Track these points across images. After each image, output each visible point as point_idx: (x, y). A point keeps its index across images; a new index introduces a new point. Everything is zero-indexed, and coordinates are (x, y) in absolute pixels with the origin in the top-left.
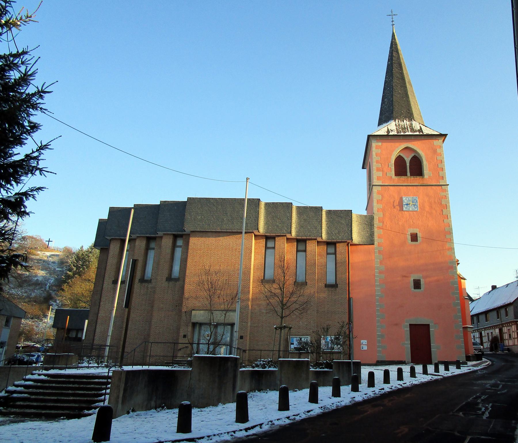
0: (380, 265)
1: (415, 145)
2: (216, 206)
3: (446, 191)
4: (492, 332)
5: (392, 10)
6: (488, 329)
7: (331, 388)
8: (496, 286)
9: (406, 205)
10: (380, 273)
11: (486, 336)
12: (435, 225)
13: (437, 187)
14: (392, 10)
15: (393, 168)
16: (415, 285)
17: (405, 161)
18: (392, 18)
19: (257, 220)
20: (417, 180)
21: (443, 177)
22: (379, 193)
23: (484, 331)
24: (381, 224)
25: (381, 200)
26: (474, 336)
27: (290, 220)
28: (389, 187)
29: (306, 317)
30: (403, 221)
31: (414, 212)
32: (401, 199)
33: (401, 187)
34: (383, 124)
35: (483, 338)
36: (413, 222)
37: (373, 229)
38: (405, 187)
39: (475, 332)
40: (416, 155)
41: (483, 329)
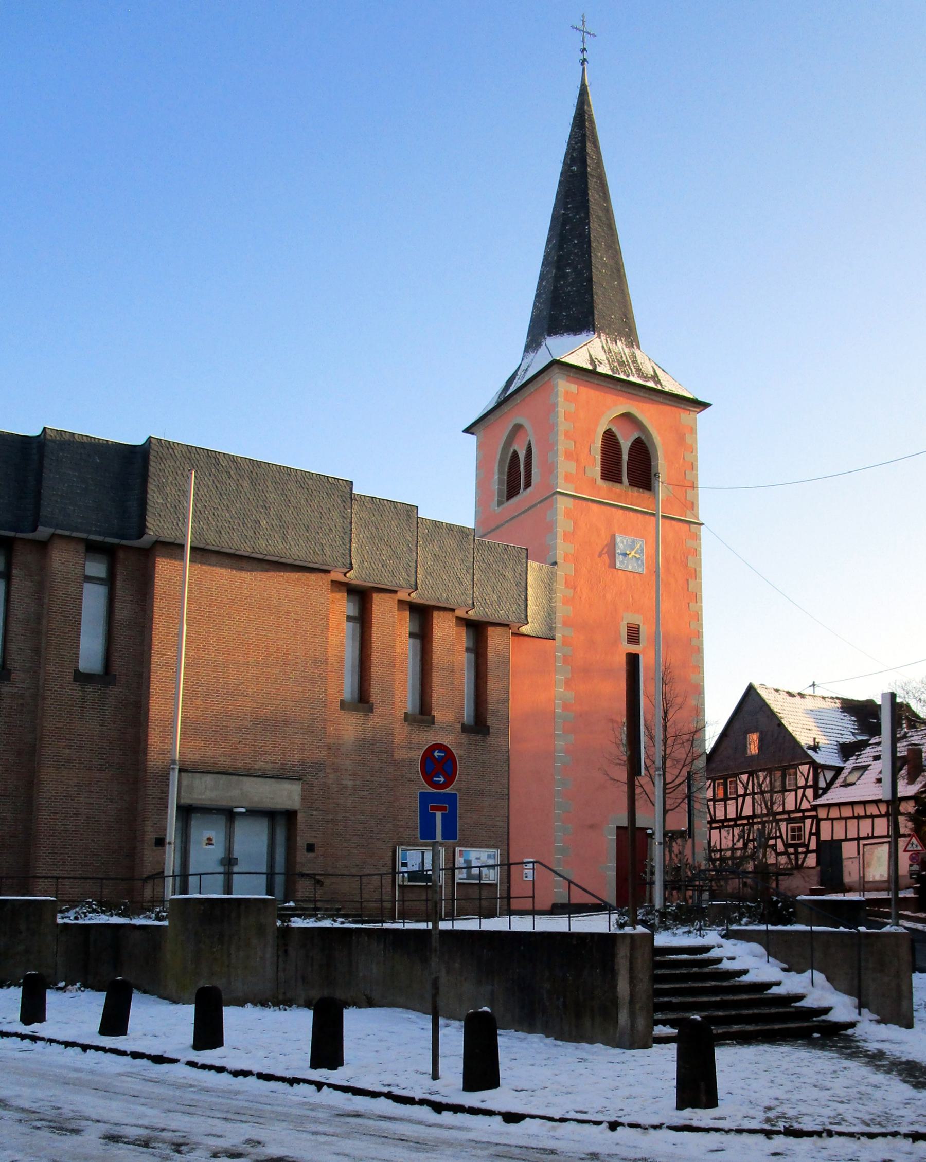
0: (565, 689)
1: (645, 412)
2: (235, 479)
3: (696, 537)
4: (407, 866)
5: (583, 16)
7: (194, 1006)
9: (621, 554)
10: (565, 707)
12: (673, 611)
13: (681, 524)
14: (583, 16)
15: (599, 457)
16: (184, 722)
17: (620, 446)
18: (583, 41)
19: (347, 540)
20: (635, 497)
21: (693, 503)
22: (568, 514)
24: (570, 593)
25: (573, 533)
27: (414, 554)
28: (590, 504)
30: (614, 592)
31: (635, 574)
32: (613, 538)
33: (614, 510)
34: (563, 333)
36: (632, 599)
37: (554, 600)
38: (621, 512)
40: (645, 441)
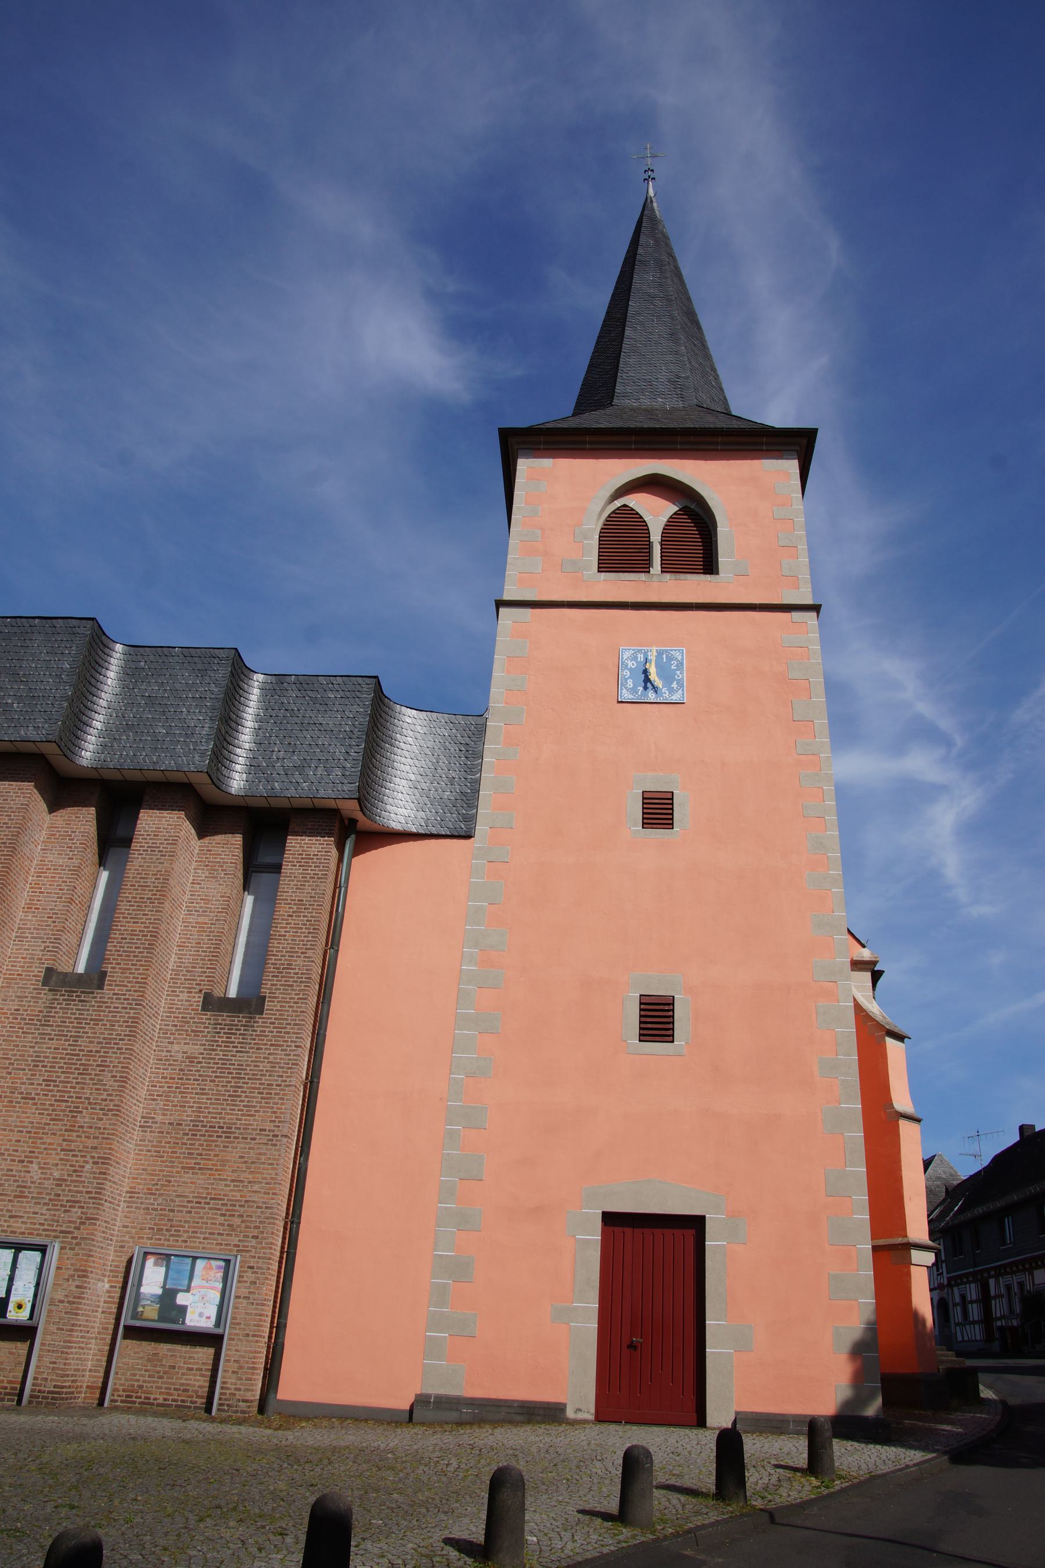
6: (1008, 1270)
8: (1034, 1126)
11: (1002, 1296)
23: (997, 1277)
26: (963, 1297)
29: (64, 1140)
35: (993, 1302)
39: (965, 1283)
41: (993, 1273)
